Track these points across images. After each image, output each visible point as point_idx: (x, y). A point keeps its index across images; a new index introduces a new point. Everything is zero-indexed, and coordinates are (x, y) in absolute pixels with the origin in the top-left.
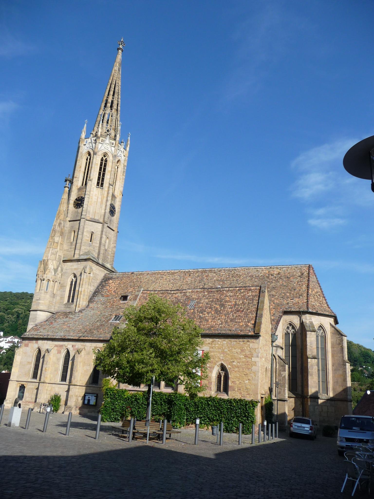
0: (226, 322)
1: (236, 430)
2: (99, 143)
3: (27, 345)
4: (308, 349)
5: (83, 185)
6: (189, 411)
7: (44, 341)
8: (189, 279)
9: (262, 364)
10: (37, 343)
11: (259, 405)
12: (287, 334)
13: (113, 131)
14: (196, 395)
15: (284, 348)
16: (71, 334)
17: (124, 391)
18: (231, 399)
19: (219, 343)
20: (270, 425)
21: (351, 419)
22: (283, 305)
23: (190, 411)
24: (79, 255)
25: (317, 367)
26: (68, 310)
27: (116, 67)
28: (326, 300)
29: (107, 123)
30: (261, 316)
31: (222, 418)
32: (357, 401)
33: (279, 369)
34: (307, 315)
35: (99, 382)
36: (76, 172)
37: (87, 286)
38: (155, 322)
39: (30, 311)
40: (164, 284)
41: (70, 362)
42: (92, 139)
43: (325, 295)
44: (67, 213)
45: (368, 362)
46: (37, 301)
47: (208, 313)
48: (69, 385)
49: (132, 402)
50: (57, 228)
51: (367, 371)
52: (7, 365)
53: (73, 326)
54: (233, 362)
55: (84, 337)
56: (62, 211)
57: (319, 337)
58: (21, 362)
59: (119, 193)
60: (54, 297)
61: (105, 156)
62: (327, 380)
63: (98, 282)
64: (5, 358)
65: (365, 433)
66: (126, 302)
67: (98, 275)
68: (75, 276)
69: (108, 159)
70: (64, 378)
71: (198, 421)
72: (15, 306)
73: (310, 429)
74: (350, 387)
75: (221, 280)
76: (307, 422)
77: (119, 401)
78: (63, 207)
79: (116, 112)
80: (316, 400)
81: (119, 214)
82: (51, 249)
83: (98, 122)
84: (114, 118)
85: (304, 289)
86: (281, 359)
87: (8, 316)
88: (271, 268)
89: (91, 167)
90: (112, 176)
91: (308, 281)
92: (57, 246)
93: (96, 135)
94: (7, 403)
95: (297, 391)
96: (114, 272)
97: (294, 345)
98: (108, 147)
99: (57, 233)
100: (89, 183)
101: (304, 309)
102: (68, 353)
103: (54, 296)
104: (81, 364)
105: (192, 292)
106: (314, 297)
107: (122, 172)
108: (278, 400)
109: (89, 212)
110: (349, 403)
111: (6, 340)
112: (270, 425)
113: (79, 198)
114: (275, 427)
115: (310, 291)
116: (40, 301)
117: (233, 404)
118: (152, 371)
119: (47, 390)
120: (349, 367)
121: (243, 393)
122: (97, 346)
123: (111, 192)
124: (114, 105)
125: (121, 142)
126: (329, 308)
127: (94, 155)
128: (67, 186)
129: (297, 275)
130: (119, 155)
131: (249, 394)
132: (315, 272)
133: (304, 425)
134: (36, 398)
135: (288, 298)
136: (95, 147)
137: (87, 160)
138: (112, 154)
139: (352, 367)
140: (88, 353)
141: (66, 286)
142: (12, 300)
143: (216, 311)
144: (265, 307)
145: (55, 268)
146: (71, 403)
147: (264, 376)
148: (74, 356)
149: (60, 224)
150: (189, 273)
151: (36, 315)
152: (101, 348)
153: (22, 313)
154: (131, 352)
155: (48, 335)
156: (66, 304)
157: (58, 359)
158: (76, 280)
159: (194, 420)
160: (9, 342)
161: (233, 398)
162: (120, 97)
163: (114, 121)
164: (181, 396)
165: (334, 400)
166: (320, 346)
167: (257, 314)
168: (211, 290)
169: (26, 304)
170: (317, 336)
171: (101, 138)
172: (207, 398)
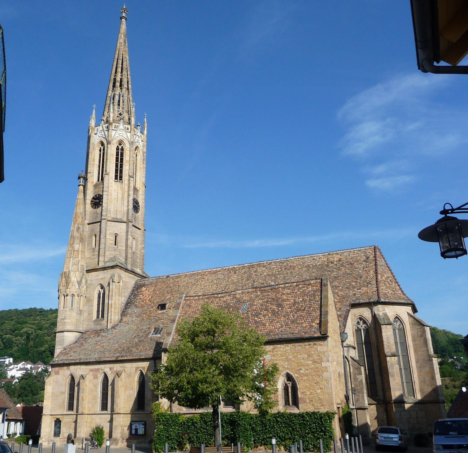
0: (287, 324)
1: (313, 448)
3: (57, 373)
4: (385, 346)
5: (98, 181)
6: (255, 431)
7: (76, 367)
8: (235, 278)
9: (334, 369)
10: (68, 369)
11: (336, 417)
12: (358, 330)
13: (127, 114)
14: (267, 412)
15: (356, 347)
16: (107, 355)
17: (177, 416)
18: (303, 413)
19: (281, 349)
20: (353, 438)
21: (446, 423)
22: (348, 297)
23: (257, 432)
24: (105, 262)
25: (398, 366)
26: (99, 328)
27: (122, 39)
28: (399, 286)
29: (119, 105)
30: (327, 313)
31: (295, 435)
32: (452, 400)
33: (353, 373)
34: (380, 306)
35: (146, 407)
36: (89, 166)
37: (117, 297)
38: (211, 335)
39: (55, 333)
40: (206, 286)
41: (110, 388)
42: (104, 126)
43: (398, 280)
44: (85, 214)
45: (459, 351)
46: (62, 321)
47: (264, 316)
48: (112, 415)
49: (189, 427)
50: (76, 234)
51: (460, 362)
52: (22, 397)
53: (108, 346)
54: (300, 369)
57: (397, 331)
58: (52, 393)
59: (141, 184)
60: (81, 314)
61: (120, 144)
62: (412, 379)
63: (129, 290)
64: (18, 388)
65: (464, 437)
66: (164, 311)
67: (128, 283)
68: (102, 287)
69: (124, 148)
70: (104, 407)
71: (274, 441)
72: (24, 326)
73: (400, 440)
74: (440, 386)
75: (272, 275)
76: (395, 432)
77: (173, 427)
78: (80, 209)
79: (127, 91)
80: (402, 404)
81: (144, 209)
82: (72, 259)
83: (107, 106)
85: (371, 276)
86: (355, 361)
87: (16, 338)
88: (329, 254)
89: (107, 159)
90: (132, 167)
91: (376, 265)
92: (78, 254)
93: (107, 122)
95: (378, 396)
96: (145, 277)
97: (368, 342)
98: (124, 134)
99: (76, 240)
100: (106, 178)
101: (375, 299)
102: (106, 377)
103: (80, 312)
104: (123, 389)
105: (242, 293)
106: (385, 284)
107: (142, 161)
108: (357, 409)
110: (442, 405)
111: (17, 367)
112: (353, 438)
113: (96, 196)
114: (358, 441)
115: (379, 277)
116: (66, 321)
117: (306, 418)
118: (218, 390)
119: (87, 422)
120: (436, 361)
121: (316, 405)
122: (139, 366)
123: (132, 185)
125: (136, 126)
126: (404, 294)
127: (108, 144)
128: (81, 183)
129: (362, 259)
130: (136, 141)
131: (323, 405)
132: (383, 254)
133: (391, 436)
135: (354, 288)
136: (108, 135)
137: (100, 151)
138: (129, 141)
139: (440, 360)
140: (129, 376)
141: (93, 300)
142: (19, 319)
143: (274, 313)
144: (329, 302)
145: (79, 280)
146: (117, 434)
147: (338, 382)
148: (114, 381)
149: (78, 228)
150: (234, 270)
152: (144, 368)
153: (32, 333)
154: (191, 372)
155: (80, 359)
156: (95, 320)
157: (95, 386)
158: (104, 291)
159: (262, 440)
160: (21, 369)
161: (305, 411)
162: (129, 73)
163: (126, 101)
164: (245, 415)
165: (424, 403)
166: (398, 341)
167: (321, 311)
168: (265, 289)
169: (36, 322)
170: (394, 330)
171: (114, 124)
172: (275, 414)
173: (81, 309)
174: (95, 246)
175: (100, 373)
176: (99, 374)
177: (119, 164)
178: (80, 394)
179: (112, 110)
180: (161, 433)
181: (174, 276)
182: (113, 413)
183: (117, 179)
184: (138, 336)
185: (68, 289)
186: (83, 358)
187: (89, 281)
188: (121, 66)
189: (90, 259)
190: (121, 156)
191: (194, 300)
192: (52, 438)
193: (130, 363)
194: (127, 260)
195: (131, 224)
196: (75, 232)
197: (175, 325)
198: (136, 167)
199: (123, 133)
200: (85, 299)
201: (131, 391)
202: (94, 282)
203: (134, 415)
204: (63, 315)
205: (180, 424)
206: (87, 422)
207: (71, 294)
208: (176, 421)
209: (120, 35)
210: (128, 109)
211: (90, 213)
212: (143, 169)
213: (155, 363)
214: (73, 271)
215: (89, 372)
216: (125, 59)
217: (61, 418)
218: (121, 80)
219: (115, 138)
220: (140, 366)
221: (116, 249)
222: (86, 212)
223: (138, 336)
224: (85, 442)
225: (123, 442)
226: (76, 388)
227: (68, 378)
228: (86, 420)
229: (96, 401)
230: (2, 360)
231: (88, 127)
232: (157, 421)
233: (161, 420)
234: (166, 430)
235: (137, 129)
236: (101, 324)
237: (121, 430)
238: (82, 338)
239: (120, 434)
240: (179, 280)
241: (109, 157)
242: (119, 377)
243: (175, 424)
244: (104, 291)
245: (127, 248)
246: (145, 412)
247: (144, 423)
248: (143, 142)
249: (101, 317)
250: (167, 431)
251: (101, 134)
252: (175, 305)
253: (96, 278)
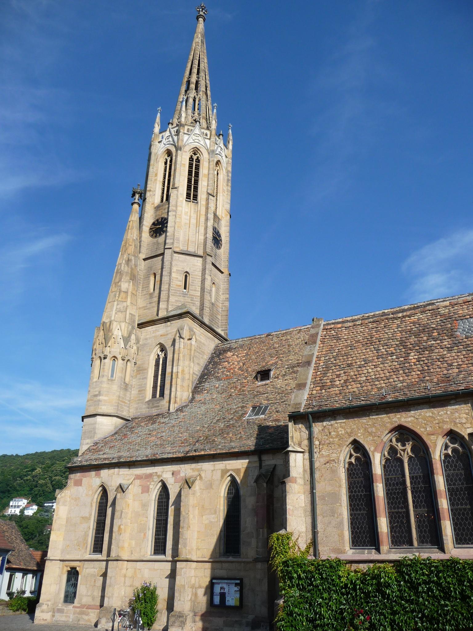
2: (184, 133)
3: (78, 483)
7: (112, 471)
10: (98, 475)
13: (204, 121)
16: (168, 449)
26: (154, 412)
27: (198, 38)
36: (149, 182)
37: (187, 363)
41: (171, 510)
46: (95, 399)
48: (174, 562)
55: (195, 451)
56: (131, 240)
61: (195, 154)
63: (206, 357)
66: (268, 382)
68: (163, 348)
69: (201, 159)
70: (159, 547)
78: (132, 234)
81: (228, 245)
82: (116, 303)
89: (175, 170)
90: (211, 182)
92: (127, 297)
94: (42, 612)
99: (124, 277)
100: (173, 193)
102: (165, 489)
103: (126, 387)
104: (197, 512)
109: (178, 239)
113: (157, 220)
116: (101, 398)
119: (125, 576)
122: (228, 467)
123: (212, 206)
127: (177, 150)
128: (136, 201)
130: (217, 152)
134: (103, 597)
136: (178, 139)
137: (166, 163)
138: (207, 150)
140: (210, 486)
141: (146, 369)
145: (126, 335)
146: (183, 604)
148: (179, 495)
149: (129, 260)
151: (95, 423)
152: (237, 471)
155: (120, 457)
156: (149, 401)
157: (145, 506)
171: (186, 127)
173: (127, 382)
174: (154, 290)
175: (153, 481)
176: (152, 483)
177: (193, 179)
178: (115, 521)
180: (296, 610)
181: (279, 333)
182: (176, 559)
183: (190, 199)
184: (224, 418)
185: (107, 348)
186: (125, 456)
187: (141, 340)
189: (145, 309)
191: (343, 329)
192: (60, 605)
193: (212, 463)
194: (203, 309)
195: (209, 259)
196: (123, 265)
197: (311, 371)
198: (217, 186)
200: (135, 369)
201: (213, 516)
202: (149, 341)
203: (218, 565)
204: (97, 389)
205: (342, 588)
206: (125, 576)
207: (112, 356)
208: (333, 580)
209: (196, 35)
211: (148, 245)
212: (226, 193)
213: (260, 460)
214: (116, 321)
215: (134, 479)
217: (79, 566)
218: (197, 83)
219: (188, 144)
220: (231, 468)
221: (187, 295)
222: (142, 242)
223: (224, 418)
224: (118, 619)
225: (194, 622)
226: (109, 511)
227: (97, 491)
228: (124, 571)
229: (145, 535)
230: (50, 504)
232: (283, 578)
233: (295, 575)
234: (307, 602)
235: (219, 139)
236: (159, 406)
237: (192, 595)
238: (127, 427)
239: (189, 603)
240: (289, 337)
241: (178, 166)
242: (190, 488)
243: (329, 588)
244: (165, 355)
245: (204, 292)
246: (240, 560)
247: (238, 582)
249: (160, 396)
250: (311, 605)
252: (285, 372)
253: (154, 335)
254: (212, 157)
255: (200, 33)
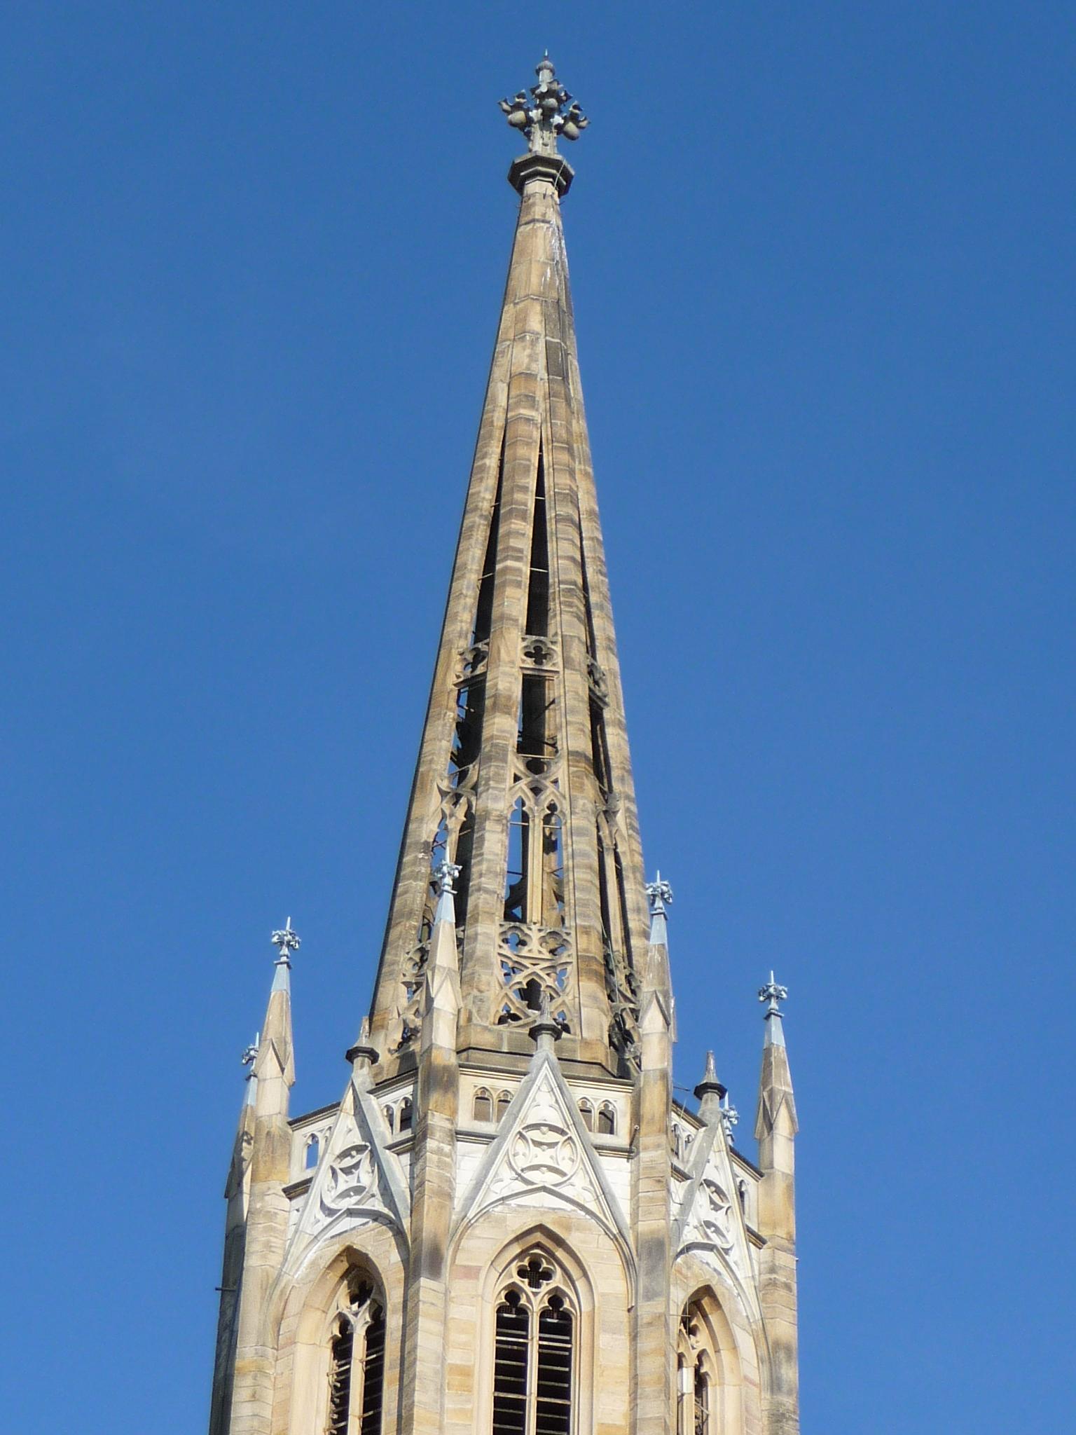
2: (458, 1135)
13: (592, 987)
27: (526, 343)
42: (375, 1106)
61: (535, 1274)
69: (579, 1304)
79: (590, 786)
83: (407, 929)
84: (579, 846)
93: (409, 1066)
124: (552, 719)
125: (690, 1095)
127: (412, 1272)
136: (417, 1186)
137: (341, 1348)
138: (618, 1238)
162: (603, 626)
163: (582, 879)
171: (469, 1085)
179: (445, 953)
188: (526, 569)
190: (542, 1391)
199: (565, 1166)
209: (509, 312)
210: (606, 940)
216: (565, 510)
218: (533, 687)
219: (484, 1213)
231: (230, 1146)
235: (700, 1123)
248: (765, 1252)
251: (345, 1182)
254: (650, 1295)
255: (541, 298)
